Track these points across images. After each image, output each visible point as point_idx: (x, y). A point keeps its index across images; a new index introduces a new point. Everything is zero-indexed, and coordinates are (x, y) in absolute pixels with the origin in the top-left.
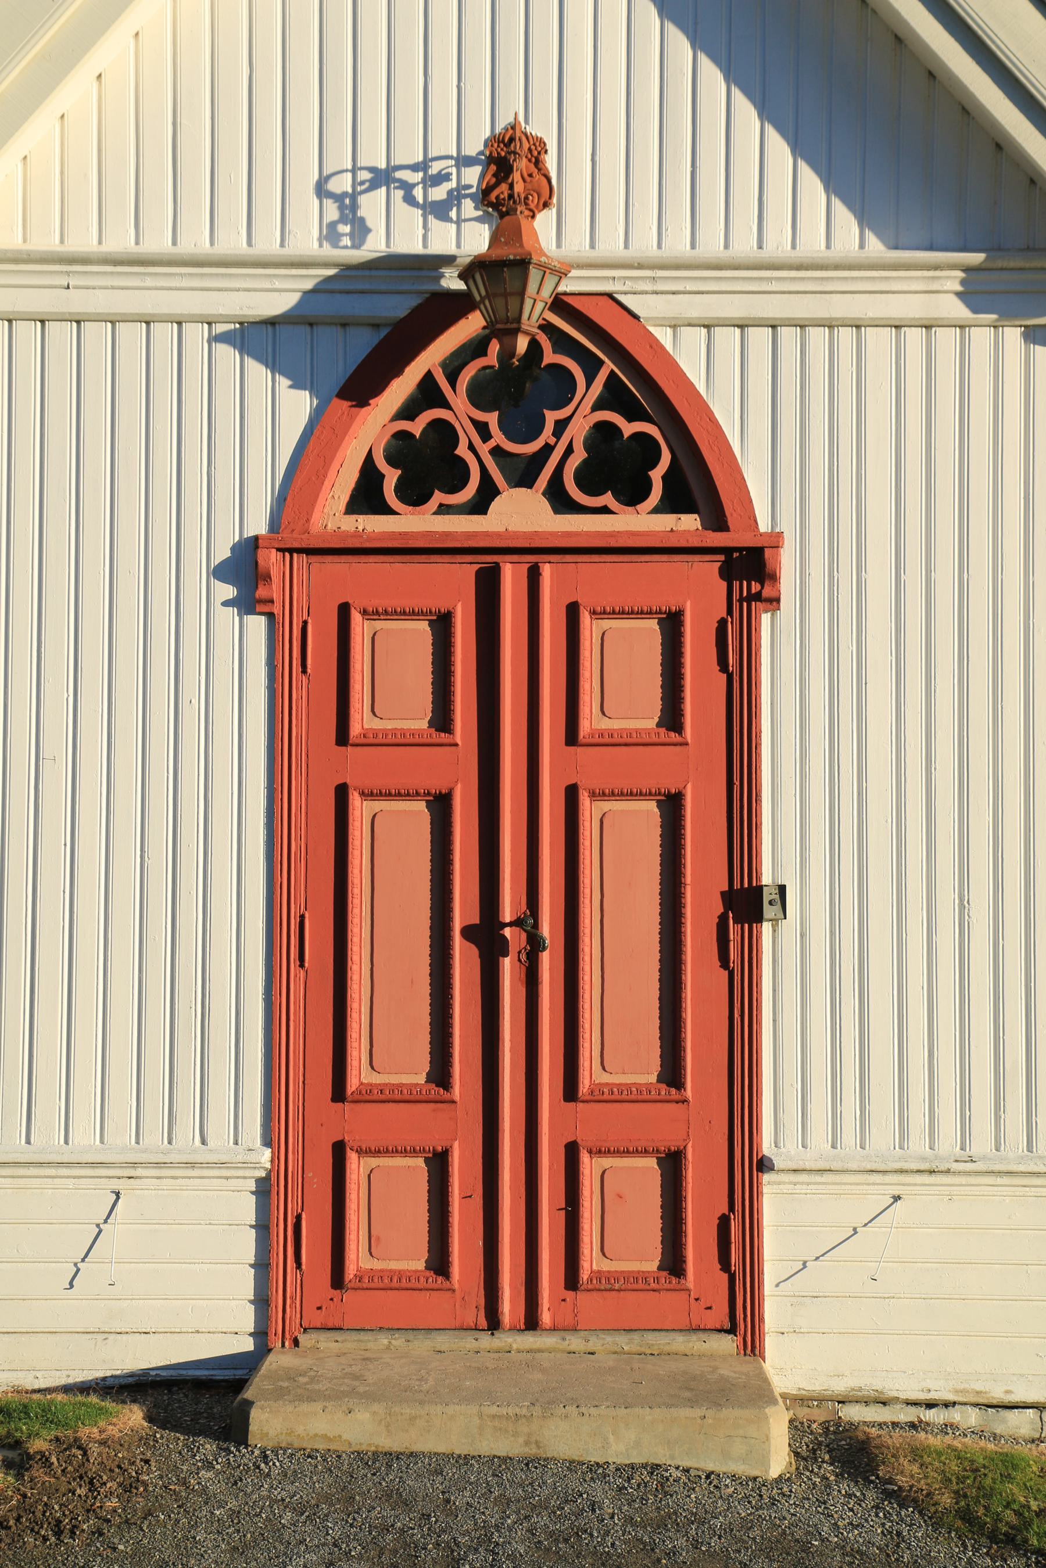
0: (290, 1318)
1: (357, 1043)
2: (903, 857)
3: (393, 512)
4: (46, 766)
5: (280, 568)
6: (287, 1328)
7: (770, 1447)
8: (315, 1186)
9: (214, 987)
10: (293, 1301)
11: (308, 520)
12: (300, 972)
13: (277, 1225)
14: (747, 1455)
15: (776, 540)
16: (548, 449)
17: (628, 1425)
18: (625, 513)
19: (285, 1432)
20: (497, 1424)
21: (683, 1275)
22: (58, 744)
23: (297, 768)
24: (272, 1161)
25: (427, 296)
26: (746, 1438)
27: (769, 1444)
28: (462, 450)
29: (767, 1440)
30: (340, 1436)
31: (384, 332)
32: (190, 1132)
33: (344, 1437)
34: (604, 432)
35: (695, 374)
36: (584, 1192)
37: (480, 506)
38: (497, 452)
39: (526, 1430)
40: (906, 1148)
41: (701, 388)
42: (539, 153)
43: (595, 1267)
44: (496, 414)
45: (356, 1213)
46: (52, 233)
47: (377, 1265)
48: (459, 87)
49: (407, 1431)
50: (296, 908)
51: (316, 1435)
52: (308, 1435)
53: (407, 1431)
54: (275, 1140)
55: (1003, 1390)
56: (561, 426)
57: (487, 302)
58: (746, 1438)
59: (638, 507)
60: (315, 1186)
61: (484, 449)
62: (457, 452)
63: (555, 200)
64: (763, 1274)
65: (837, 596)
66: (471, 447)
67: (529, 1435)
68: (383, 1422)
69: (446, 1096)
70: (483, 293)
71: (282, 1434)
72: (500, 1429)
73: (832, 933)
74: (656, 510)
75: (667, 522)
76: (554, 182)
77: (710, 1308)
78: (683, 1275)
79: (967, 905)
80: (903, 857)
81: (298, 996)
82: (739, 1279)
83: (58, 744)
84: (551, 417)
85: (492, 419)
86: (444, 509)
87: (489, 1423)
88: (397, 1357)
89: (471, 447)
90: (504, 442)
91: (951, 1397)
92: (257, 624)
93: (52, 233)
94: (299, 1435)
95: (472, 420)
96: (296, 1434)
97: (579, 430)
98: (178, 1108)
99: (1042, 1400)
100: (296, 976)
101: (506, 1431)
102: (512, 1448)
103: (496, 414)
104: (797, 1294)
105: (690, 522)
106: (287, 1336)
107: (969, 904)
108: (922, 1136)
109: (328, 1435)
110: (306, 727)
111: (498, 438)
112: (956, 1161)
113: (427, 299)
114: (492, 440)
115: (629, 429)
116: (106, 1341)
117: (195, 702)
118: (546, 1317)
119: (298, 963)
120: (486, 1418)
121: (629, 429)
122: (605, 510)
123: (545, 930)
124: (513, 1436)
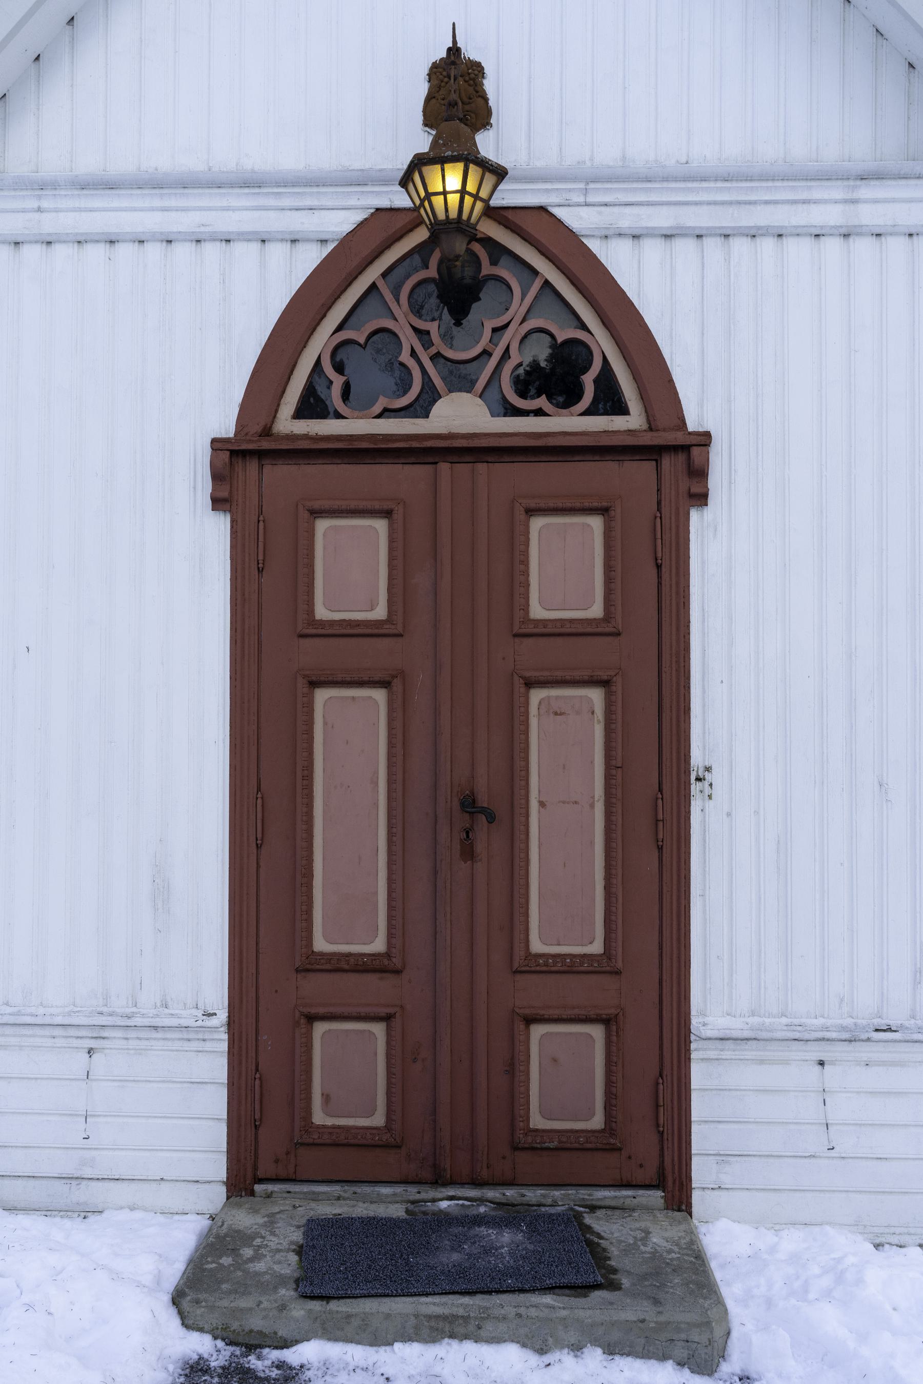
26: (687, 1341)
29: (710, 1344)
74: (587, 413)
86: (386, 413)
89: (413, 353)
122: (539, 412)
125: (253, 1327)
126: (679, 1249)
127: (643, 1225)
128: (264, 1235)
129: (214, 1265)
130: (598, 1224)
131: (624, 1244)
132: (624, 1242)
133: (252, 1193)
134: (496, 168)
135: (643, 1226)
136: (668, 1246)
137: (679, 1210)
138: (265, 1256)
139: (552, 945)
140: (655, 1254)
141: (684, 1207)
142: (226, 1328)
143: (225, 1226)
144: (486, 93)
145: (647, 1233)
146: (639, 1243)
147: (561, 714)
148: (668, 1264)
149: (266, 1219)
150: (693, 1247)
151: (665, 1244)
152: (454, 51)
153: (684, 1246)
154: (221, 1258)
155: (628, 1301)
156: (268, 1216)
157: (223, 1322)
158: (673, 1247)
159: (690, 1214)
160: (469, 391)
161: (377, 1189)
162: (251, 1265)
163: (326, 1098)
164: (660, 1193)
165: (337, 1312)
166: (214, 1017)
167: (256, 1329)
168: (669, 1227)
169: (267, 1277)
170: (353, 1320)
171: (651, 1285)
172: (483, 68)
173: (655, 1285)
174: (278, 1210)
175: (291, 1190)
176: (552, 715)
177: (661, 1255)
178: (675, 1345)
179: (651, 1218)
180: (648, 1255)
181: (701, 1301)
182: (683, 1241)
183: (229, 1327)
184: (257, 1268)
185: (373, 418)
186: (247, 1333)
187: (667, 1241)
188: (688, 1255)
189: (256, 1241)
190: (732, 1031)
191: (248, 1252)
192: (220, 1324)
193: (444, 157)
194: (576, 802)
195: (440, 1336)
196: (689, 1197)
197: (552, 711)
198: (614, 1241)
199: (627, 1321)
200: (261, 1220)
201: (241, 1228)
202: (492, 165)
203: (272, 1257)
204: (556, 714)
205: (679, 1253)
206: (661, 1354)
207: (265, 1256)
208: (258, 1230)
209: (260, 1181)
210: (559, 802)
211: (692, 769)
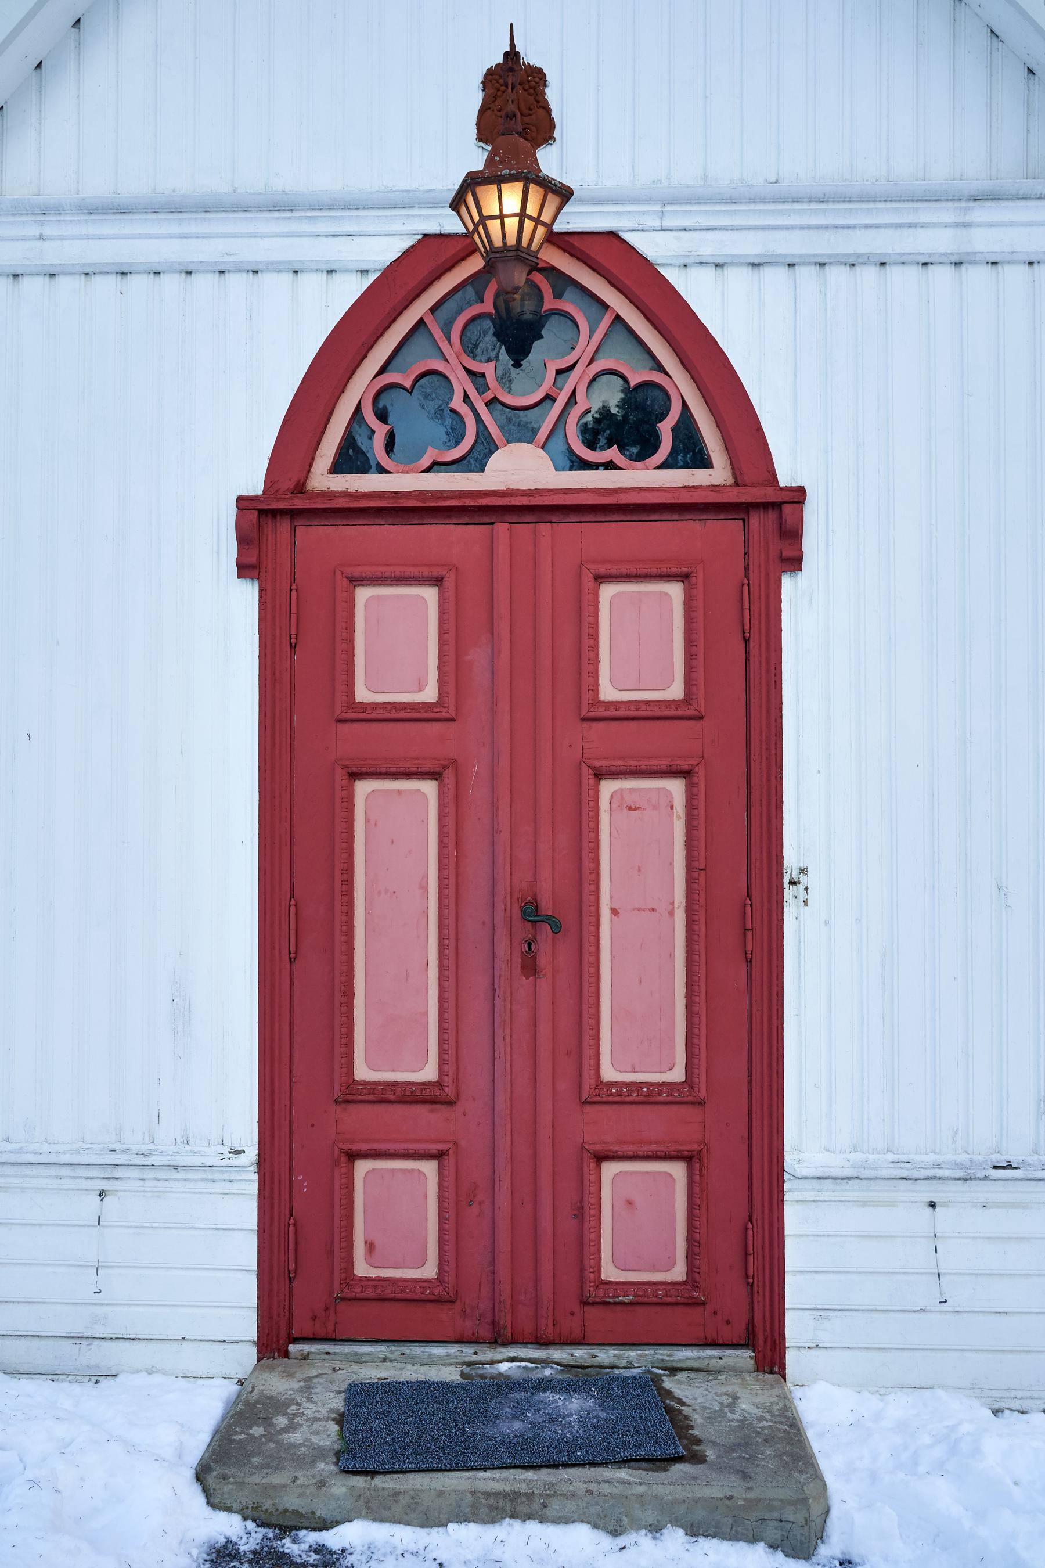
8: (305, 1190)
14: (782, 1541)
15: (798, 495)
16: (550, 398)
17: (644, 1505)
19: (250, 1506)
20: (492, 1502)
25: (420, 237)
26: (781, 1521)
30: (313, 1513)
31: (372, 278)
33: (318, 1514)
49: (390, 1509)
51: (286, 1511)
52: (277, 1510)
53: (390, 1509)
57: (481, 229)
58: (781, 1521)
60: (305, 1190)
66: (466, 398)
68: (362, 1497)
71: (247, 1508)
74: (663, 466)
87: (484, 1502)
94: (266, 1510)
96: (264, 1509)
101: (503, 1510)
104: (819, 1307)
109: (300, 1511)
112: (995, 1167)
113: (419, 241)
116: (90, 1347)
120: (480, 1495)
122: (610, 465)
125: (287, 1506)
126: (772, 1416)
127: (730, 1389)
128: (299, 1401)
129: (243, 1436)
131: (708, 1411)
132: (710, 1409)
136: (759, 1413)
142: (257, 1508)
145: (735, 1398)
146: (726, 1410)
147: (636, 809)
148: (759, 1433)
149: (302, 1384)
150: (787, 1414)
151: (756, 1411)
152: (512, 55)
153: (777, 1413)
154: (251, 1428)
155: (714, 1475)
156: (304, 1380)
157: (254, 1501)
159: (784, 1378)
163: (370, 1247)
164: (750, 1353)
167: (291, 1508)
168: (760, 1392)
169: (304, 1449)
172: (545, 75)
175: (330, 1351)
176: (625, 810)
177: (751, 1424)
182: (776, 1408)
183: (260, 1507)
184: (292, 1440)
186: (281, 1513)
187: (758, 1408)
188: (781, 1423)
189: (291, 1409)
190: (832, 1170)
191: (281, 1421)
193: (501, 175)
194: (653, 910)
196: (783, 1357)
198: (698, 1407)
200: (296, 1385)
201: (274, 1394)
203: (309, 1427)
204: (630, 809)
205: (771, 1421)
208: (293, 1396)
209: (295, 1340)
211: (785, 871)
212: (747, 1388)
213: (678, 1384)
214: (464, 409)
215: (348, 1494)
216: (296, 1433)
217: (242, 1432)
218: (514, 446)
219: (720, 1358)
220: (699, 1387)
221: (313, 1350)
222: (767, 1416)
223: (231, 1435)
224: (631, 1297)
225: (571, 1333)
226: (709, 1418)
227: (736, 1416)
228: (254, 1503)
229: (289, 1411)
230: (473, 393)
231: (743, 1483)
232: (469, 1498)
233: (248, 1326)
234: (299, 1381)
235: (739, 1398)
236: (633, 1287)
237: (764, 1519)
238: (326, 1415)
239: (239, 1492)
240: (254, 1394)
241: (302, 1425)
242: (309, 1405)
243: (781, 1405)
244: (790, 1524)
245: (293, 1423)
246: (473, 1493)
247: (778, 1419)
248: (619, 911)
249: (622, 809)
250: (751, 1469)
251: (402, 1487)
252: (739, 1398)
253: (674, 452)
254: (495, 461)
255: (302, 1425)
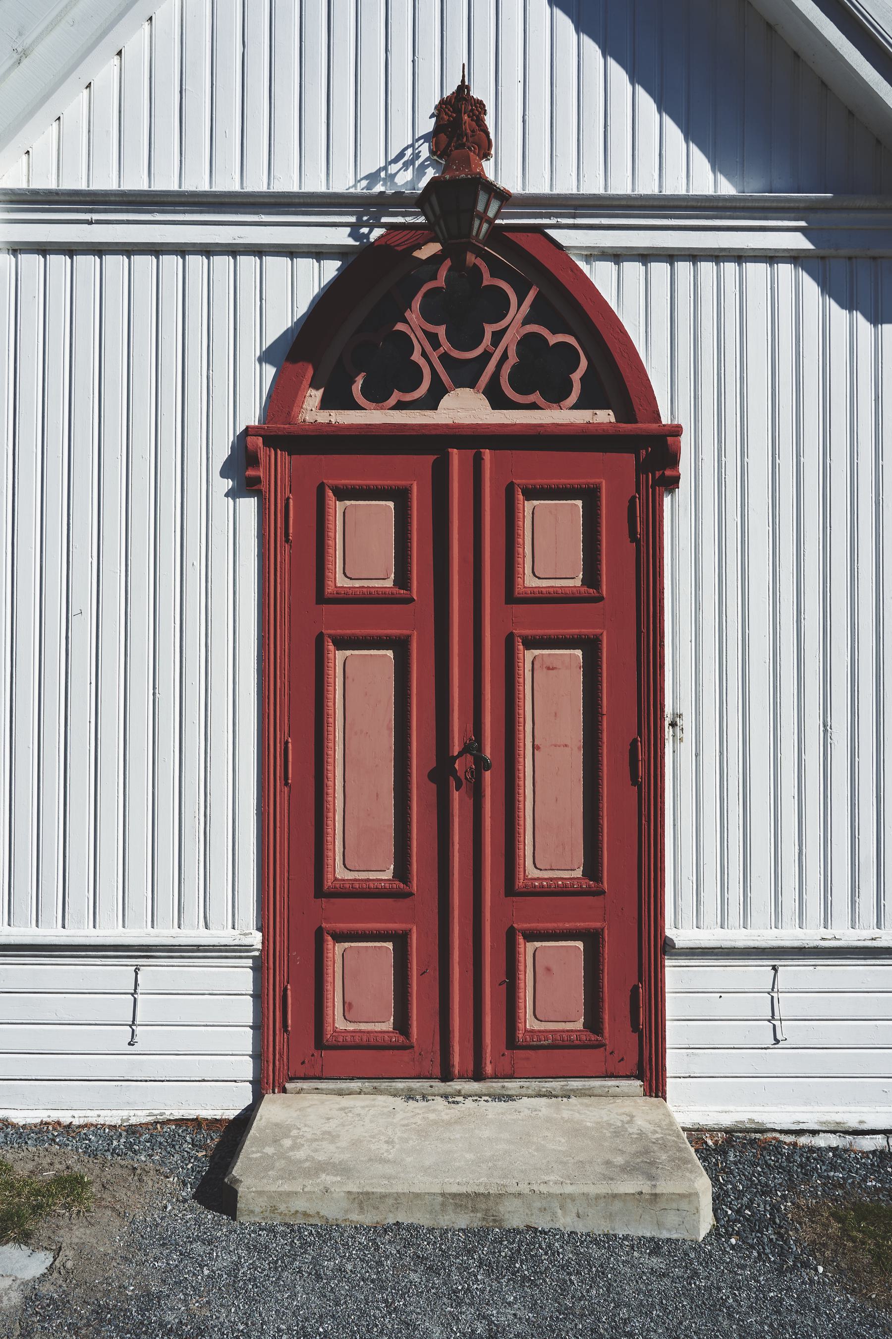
0: (279, 1069)
1: (332, 846)
2: (778, 691)
3: (361, 408)
4: (75, 621)
5: (266, 453)
6: (277, 1078)
7: (699, 1218)
9: (213, 799)
10: (281, 1056)
11: (289, 413)
12: (284, 789)
13: (267, 995)
15: (676, 431)
18: (550, 408)
20: (457, 1201)
21: (601, 1033)
22: (83, 598)
23: (281, 619)
24: (263, 943)
26: (678, 1210)
27: (699, 1215)
28: (416, 357)
29: (697, 1212)
30: (318, 1213)
32: (195, 919)
34: (529, 343)
35: (608, 294)
36: (519, 967)
37: (431, 402)
38: (445, 358)
39: (483, 1206)
40: (780, 927)
41: (613, 305)
42: (480, 113)
43: (528, 1027)
44: (444, 327)
45: (332, 984)
46: (80, 180)
47: (351, 1027)
48: (413, 61)
50: (281, 735)
51: (297, 1212)
54: (265, 926)
55: (857, 1121)
56: (498, 336)
57: (442, 223)
58: (678, 1210)
59: (562, 404)
61: (434, 356)
62: (412, 358)
63: (493, 152)
64: (665, 1031)
65: (725, 478)
67: (487, 1210)
69: (406, 889)
70: (438, 211)
72: (461, 1206)
73: (721, 753)
74: (575, 407)
75: (582, 417)
76: (492, 136)
77: (622, 1059)
78: (601, 1033)
79: (829, 730)
80: (778, 691)
81: (283, 807)
82: (646, 1036)
83: (83, 598)
84: (489, 329)
85: (441, 331)
86: (401, 406)
88: (367, 1106)
89: (424, 354)
90: (450, 349)
91: (816, 1127)
92: (249, 506)
93: (80, 180)
95: (425, 332)
97: (511, 340)
98: (185, 900)
99: (889, 1128)
100: (281, 791)
102: (471, 1222)
103: (444, 327)
105: (605, 417)
106: (277, 1084)
107: (831, 729)
108: (793, 918)
110: (288, 584)
111: (446, 346)
114: (441, 348)
115: (553, 339)
117: (197, 564)
118: (489, 1069)
119: (283, 782)
121: (553, 339)
122: (533, 406)
123: (488, 752)
124: (472, 1211)
125: (298, 1209)
126: (662, 1130)
127: (627, 1110)
128: (299, 1127)
129: (259, 1155)
130: (588, 1110)
131: (613, 1127)
132: (613, 1125)
133: (284, 1090)
134: (502, 191)
135: (628, 1111)
136: (652, 1127)
137: (657, 1096)
138: (303, 1145)
139: (546, 870)
140: (641, 1134)
141: (660, 1094)
142: (274, 1210)
143: (264, 1120)
144: (487, 127)
145: (632, 1117)
146: (627, 1126)
147: (553, 669)
148: (654, 1143)
149: (298, 1112)
150: (672, 1128)
151: (649, 1126)
152: (463, 89)
153: (665, 1128)
154: (264, 1149)
155: (625, 1176)
156: (299, 1110)
157: (272, 1205)
158: (656, 1129)
159: (665, 1100)
160: (472, 385)
161: (394, 1084)
162: (291, 1153)
163: (347, 1006)
164: (639, 1083)
165: (373, 1193)
166: (250, 936)
167: (300, 1210)
168: (650, 1111)
169: (307, 1164)
170: (387, 1200)
171: (642, 1162)
172: (484, 106)
173: (646, 1162)
174: (308, 1105)
175: (319, 1087)
176: (545, 670)
177: (647, 1136)
178: (667, 1214)
179: (633, 1104)
180: (636, 1136)
181: (688, 1174)
182: (664, 1123)
183: (276, 1209)
184: (298, 1157)
185: (388, 409)
186: (293, 1214)
187: (650, 1124)
188: (670, 1135)
189: (293, 1132)
190: (701, 942)
191: (287, 1143)
192: (269, 1206)
193: (459, 179)
194: (566, 745)
195: (463, 1212)
196: (664, 1085)
197: (545, 666)
198: (605, 1124)
199: (626, 1194)
200: (295, 1114)
201: (279, 1121)
202: (499, 188)
203: (309, 1146)
204: (548, 668)
205: (662, 1133)
206: (655, 1222)
207: (303, 1145)
208: (293, 1123)
209: (291, 1079)
210: (551, 745)
211: (666, 716)
212: (639, 1109)
213: (587, 1107)
214: (422, 362)
215: (346, 1197)
216: (299, 1151)
217: (258, 1152)
218: (458, 390)
219: (618, 1087)
220: (604, 1109)
221: (304, 1087)
222: (658, 1129)
223: (249, 1154)
224: (550, 1041)
225: (504, 1070)
226: (615, 1132)
227: (635, 1130)
228: (271, 1207)
229: (292, 1134)
230: (428, 348)
231: (649, 1183)
232: (440, 1199)
233: (246, 1068)
234: (296, 1111)
235: (635, 1116)
236: (551, 1034)
237: (665, 1209)
238: (321, 1136)
239: (259, 1198)
240: (262, 1121)
241: (303, 1145)
242: (306, 1129)
243: (667, 1121)
244: (686, 1212)
245: (296, 1143)
246: (443, 1195)
247: (667, 1132)
248: (540, 746)
249: (543, 668)
250: (653, 1171)
251: (387, 1191)
252: (635, 1116)
253: (580, 398)
254: (446, 401)
255: (303, 1145)
